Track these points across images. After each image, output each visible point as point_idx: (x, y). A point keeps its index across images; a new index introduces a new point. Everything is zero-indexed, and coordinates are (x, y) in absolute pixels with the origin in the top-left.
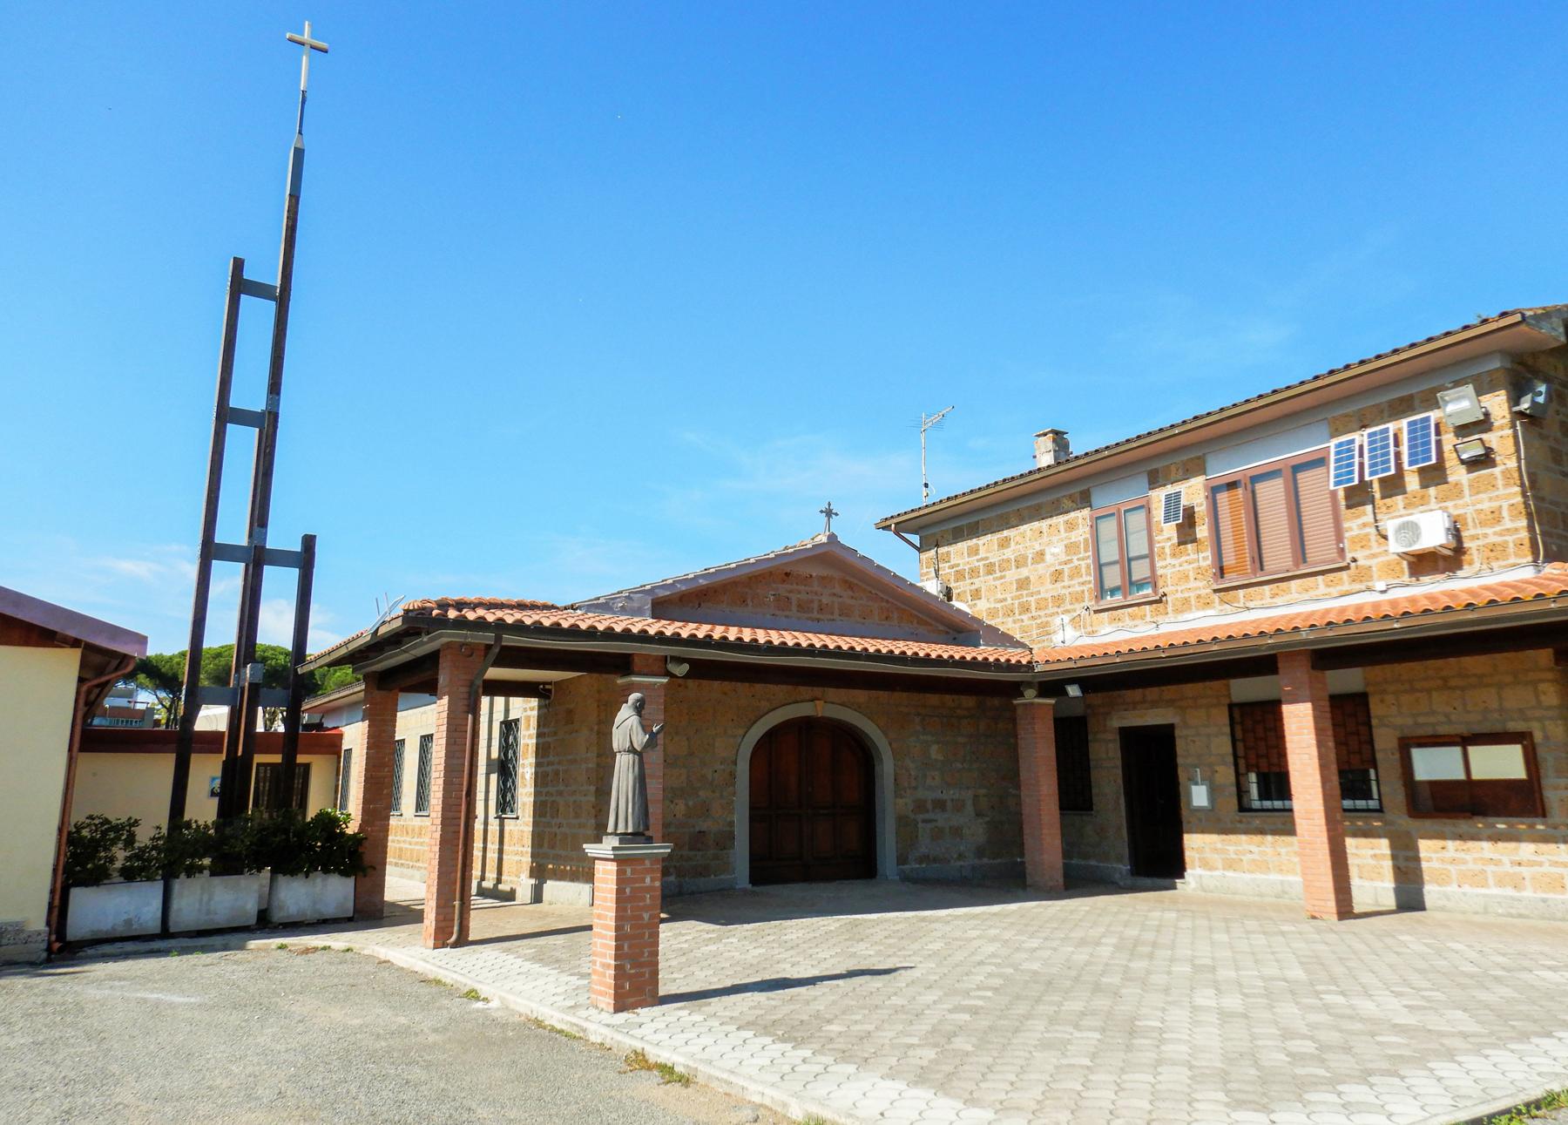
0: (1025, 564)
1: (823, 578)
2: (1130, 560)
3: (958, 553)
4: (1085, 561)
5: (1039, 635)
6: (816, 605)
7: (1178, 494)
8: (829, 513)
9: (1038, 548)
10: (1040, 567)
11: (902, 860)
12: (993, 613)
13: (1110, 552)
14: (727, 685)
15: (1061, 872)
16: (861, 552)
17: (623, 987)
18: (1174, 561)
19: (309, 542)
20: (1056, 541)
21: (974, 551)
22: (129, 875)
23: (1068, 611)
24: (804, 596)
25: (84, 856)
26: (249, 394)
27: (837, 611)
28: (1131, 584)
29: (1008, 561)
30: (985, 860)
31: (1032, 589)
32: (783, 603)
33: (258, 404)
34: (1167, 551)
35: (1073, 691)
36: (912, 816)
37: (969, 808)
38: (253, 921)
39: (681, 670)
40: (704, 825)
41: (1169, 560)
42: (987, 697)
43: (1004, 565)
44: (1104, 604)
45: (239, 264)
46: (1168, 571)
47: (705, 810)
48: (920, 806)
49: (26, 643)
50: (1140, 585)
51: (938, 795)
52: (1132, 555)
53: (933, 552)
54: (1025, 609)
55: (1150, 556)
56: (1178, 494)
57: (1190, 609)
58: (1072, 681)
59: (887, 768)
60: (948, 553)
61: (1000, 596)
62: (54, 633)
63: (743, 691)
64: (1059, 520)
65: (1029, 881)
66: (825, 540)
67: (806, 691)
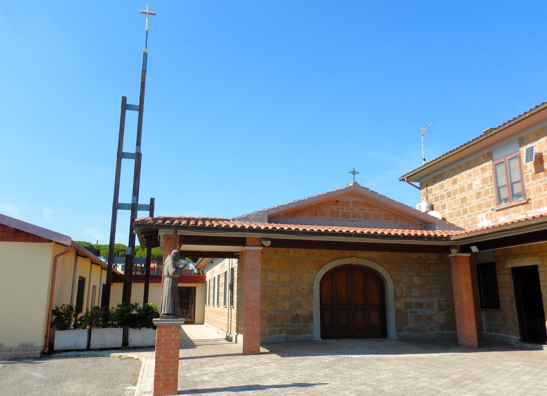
0: (464, 191)
1: (355, 202)
2: (512, 184)
3: (435, 189)
4: (491, 187)
5: (472, 224)
6: (351, 215)
7: (532, 148)
8: (354, 173)
9: (469, 182)
10: (471, 191)
11: (399, 330)
12: (451, 215)
13: (502, 181)
14: (308, 251)
15: (476, 338)
16: (371, 189)
17: (158, 385)
18: (534, 182)
19: (152, 200)
20: (476, 180)
21: (442, 187)
22: (76, 327)
23: (484, 212)
24: (345, 211)
25: (59, 319)
26: (129, 147)
27: (362, 217)
28: (514, 196)
29: (457, 190)
30: (445, 332)
31: (468, 202)
32: (335, 215)
33: (133, 150)
34: (530, 177)
35: (474, 249)
36: (404, 310)
37: (436, 306)
38: (120, 346)
39: (268, 243)
40: (299, 312)
41: (531, 182)
42: (432, 252)
43: (455, 192)
44: (501, 207)
45: (124, 99)
46: (531, 188)
47: (299, 306)
48: (408, 305)
49: (35, 241)
50: (519, 196)
51: (418, 300)
52: (513, 181)
53: (425, 190)
54: (465, 212)
55: (521, 181)
56: (532, 148)
57: (542, 206)
58: (473, 244)
59: (390, 287)
60: (431, 189)
61: (454, 207)
62: (39, 237)
63: (316, 253)
64: (478, 168)
65: (459, 343)
66: (351, 184)
67: (347, 253)
